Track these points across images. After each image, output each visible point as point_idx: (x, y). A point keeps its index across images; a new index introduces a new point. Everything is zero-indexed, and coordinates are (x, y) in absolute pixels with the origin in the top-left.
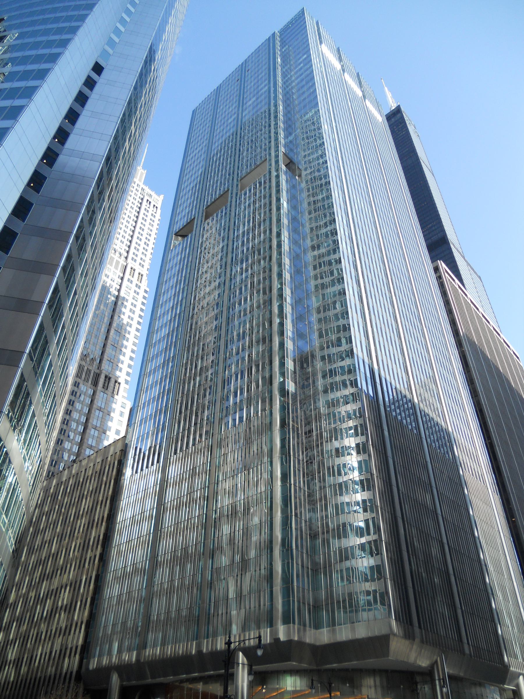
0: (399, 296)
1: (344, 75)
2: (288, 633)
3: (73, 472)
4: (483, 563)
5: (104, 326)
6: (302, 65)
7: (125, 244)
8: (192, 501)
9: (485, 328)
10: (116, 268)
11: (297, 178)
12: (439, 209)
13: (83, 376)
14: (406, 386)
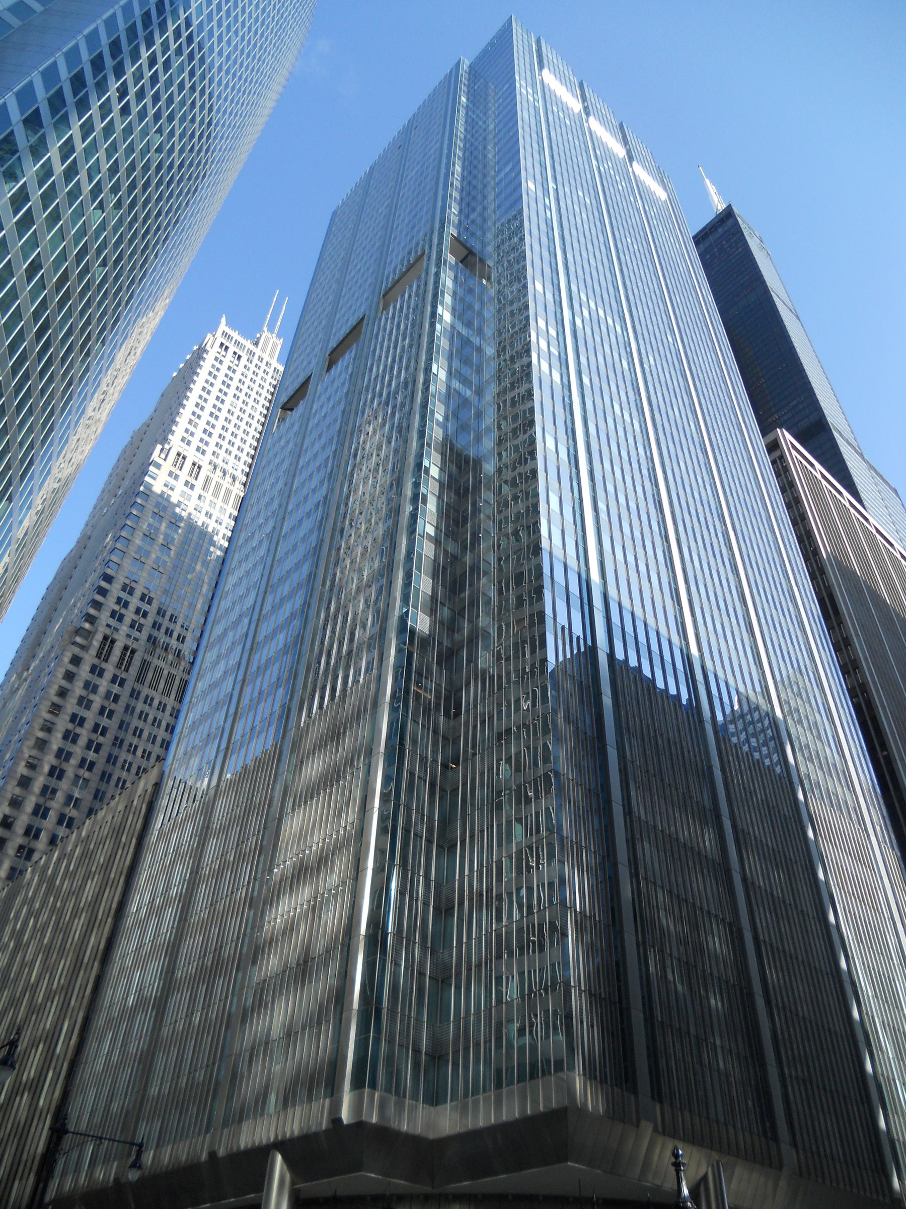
0: (758, 545)
1: (631, 166)
2: (357, 1107)
3: (84, 834)
4: (845, 978)
5: (201, 601)
6: (501, 101)
7: (242, 461)
8: (241, 857)
9: (828, 504)
10: (226, 501)
11: (484, 282)
12: (808, 373)
13: (161, 686)
14: (758, 689)
